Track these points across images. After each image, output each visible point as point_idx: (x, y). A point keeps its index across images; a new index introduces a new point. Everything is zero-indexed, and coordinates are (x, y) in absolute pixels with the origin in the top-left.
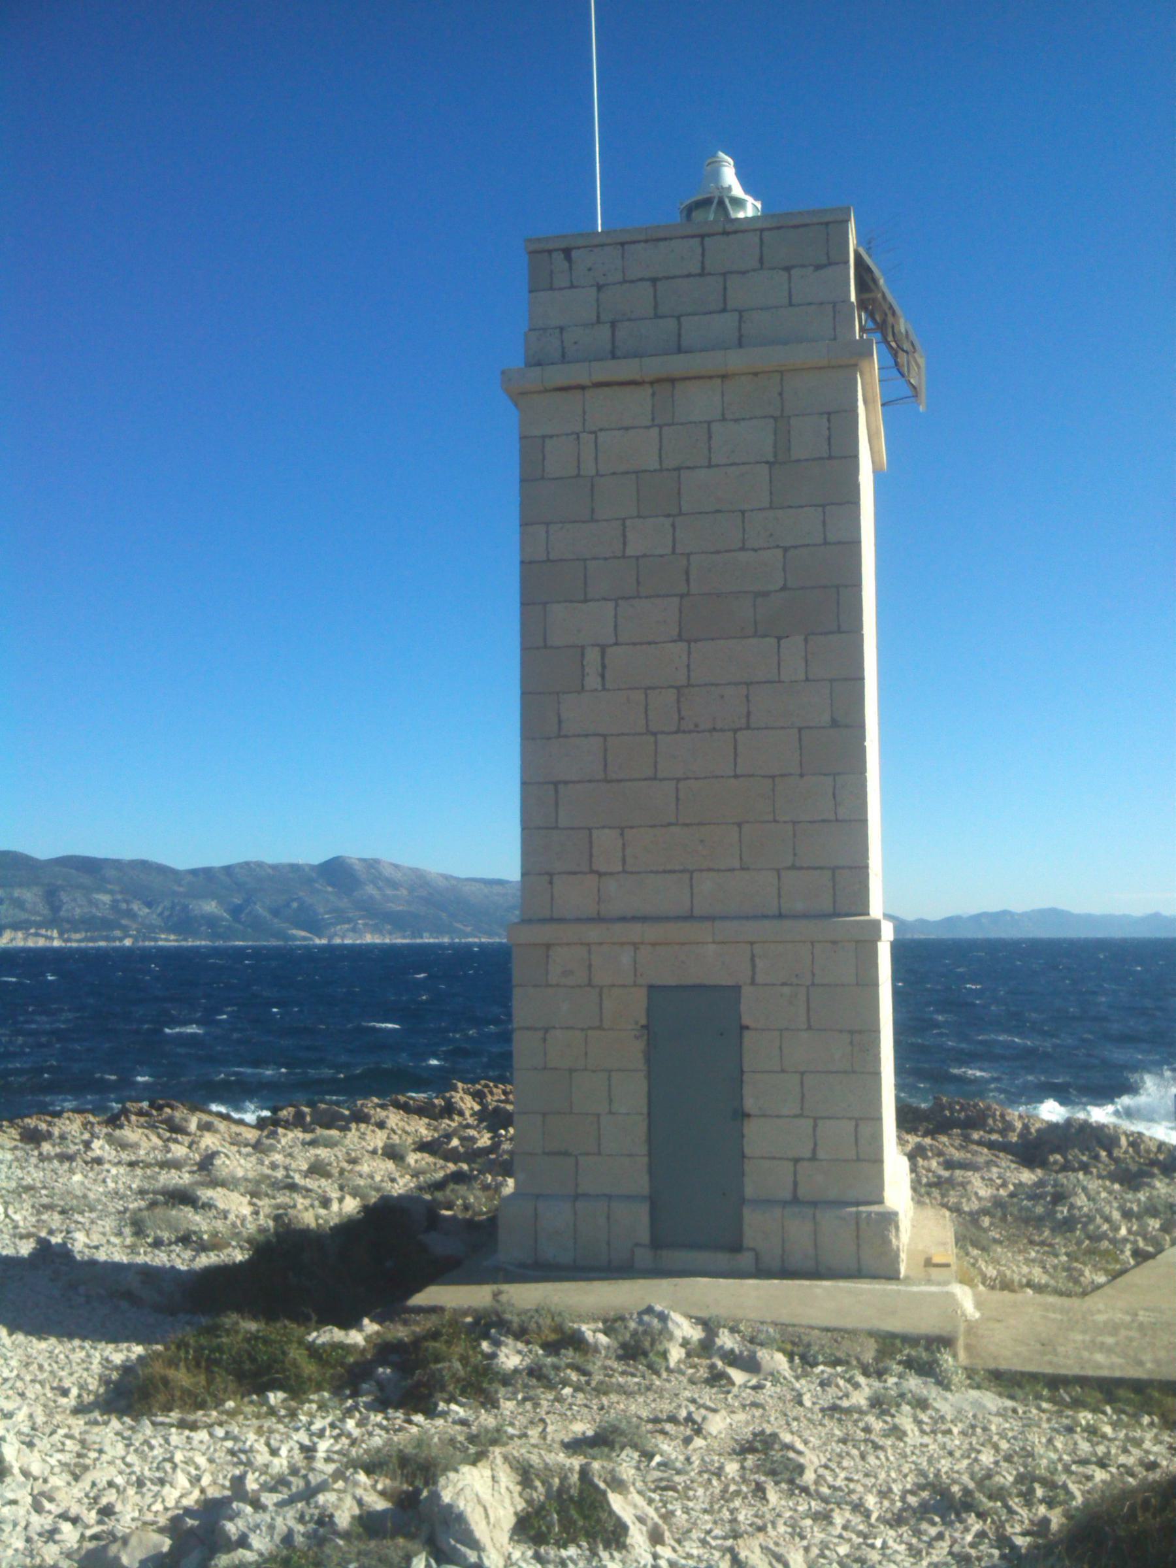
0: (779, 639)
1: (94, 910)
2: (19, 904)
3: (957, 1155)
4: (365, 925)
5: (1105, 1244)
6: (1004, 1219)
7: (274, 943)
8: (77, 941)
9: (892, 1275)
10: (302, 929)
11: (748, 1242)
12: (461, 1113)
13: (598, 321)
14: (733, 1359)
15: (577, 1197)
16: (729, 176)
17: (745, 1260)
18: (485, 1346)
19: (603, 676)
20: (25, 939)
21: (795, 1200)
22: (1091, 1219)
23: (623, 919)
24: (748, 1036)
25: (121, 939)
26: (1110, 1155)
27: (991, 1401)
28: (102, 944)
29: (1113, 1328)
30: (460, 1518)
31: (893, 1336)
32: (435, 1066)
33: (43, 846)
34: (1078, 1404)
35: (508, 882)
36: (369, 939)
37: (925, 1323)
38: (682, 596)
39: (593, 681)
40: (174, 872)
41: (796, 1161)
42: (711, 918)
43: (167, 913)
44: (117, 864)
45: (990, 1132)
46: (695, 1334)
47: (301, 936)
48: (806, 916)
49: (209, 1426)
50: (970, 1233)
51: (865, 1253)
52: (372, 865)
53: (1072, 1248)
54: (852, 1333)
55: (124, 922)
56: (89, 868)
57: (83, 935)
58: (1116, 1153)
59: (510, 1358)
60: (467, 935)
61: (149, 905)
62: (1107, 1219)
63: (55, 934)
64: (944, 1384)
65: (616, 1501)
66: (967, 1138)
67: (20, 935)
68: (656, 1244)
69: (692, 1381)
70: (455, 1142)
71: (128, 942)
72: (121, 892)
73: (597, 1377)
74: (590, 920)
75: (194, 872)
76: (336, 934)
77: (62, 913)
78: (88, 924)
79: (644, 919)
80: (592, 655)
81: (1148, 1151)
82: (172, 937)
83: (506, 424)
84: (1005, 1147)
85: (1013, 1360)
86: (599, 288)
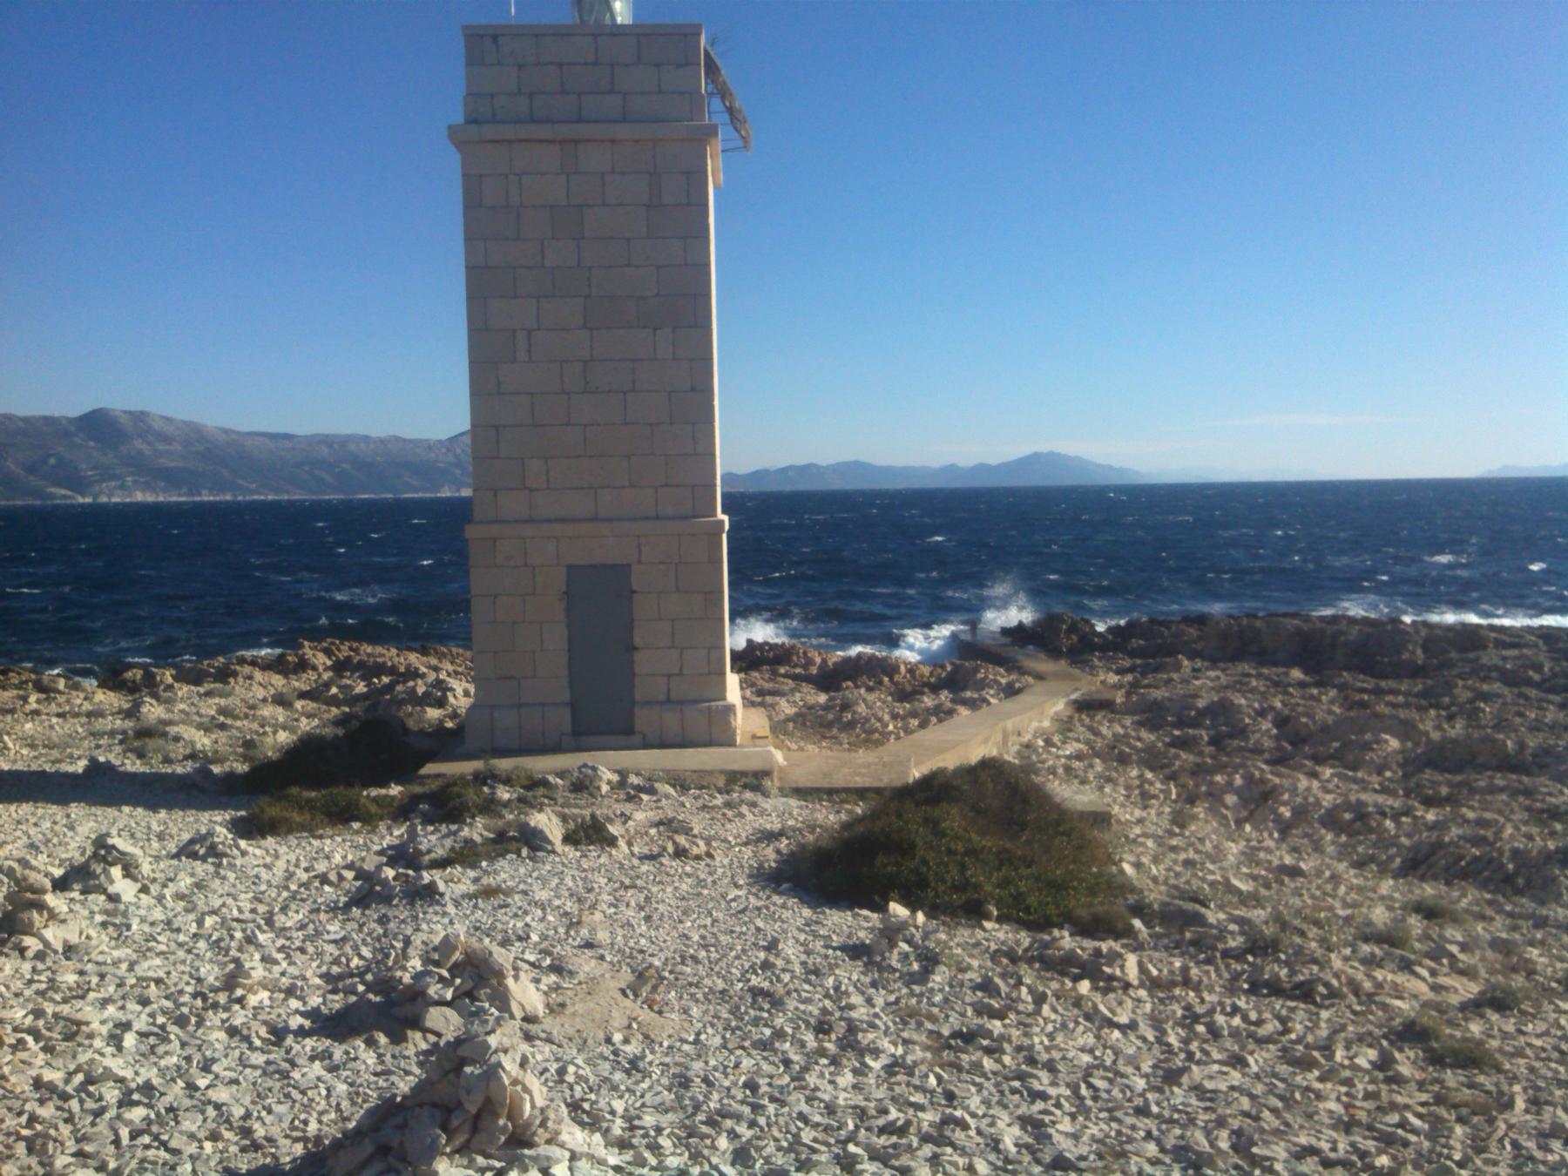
0: (655, 329)
3: (767, 686)
4: (134, 482)
6: (804, 724)
7: (30, 501)
9: (732, 743)
10: (59, 485)
11: (638, 727)
12: (315, 668)
14: (639, 789)
15: (520, 706)
17: (637, 739)
18: (486, 789)
21: (669, 701)
22: (867, 720)
23: (549, 521)
24: (636, 597)
26: (891, 680)
29: (868, 765)
30: (541, 832)
31: (735, 772)
34: (844, 801)
36: (139, 497)
41: (669, 676)
42: (610, 520)
45: (795, 666)
46: (615, 778)
47: (61, 495)
48: (674, 518)
51: (717, 732)
52: (140, 417)
53: (853, 739)
54: (711, 773)
58: (896, 678)
59: (504, 794)
60: (252, 492)
62: (880, 720)
64: (766, 794)
65: (611, 829)
66: (775, 673)
68: (576, 733)
69: (617, 801)
70: (334, 690)
74: (525, 522)
76: (101, 492)
79: (563, 520)
81: (922, 676)
83: (452, 162)
84: (808, 679)
85: (804, 782)
86: (520, 67)
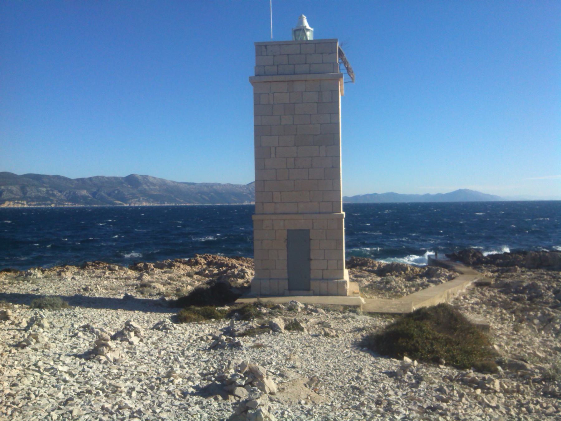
1: (39, 194)
2: (11, 192)
3: (359, 274)
4: (143, 199)
5: (399, 293)
6: (372, 288)
7: (109, 206)
8: (33, 205)
9: (346, 295)
11: (312, 288)
12: (201, 264)
13: (274, 65)
14: (312, 310)
15: (270, 279)
16: (306, 23)
17: (311, 292)
19: (275, 154)
20: (14, 205)
21: (323, 279)
22: (396, 287)
24: (312, 242)
25: (50, 205)
26: (405, 273)
27: (368, 317)
28: (43, 206)
29: (396, 305)
30: (277, 325)
32: (368, 247)
33: (19, 171)
34: (387, 318)
35: (196, 184)
36: (144, 204)
37: (354, 303)
38: (295, 135)
39: (273, 155)
40: (70, 180)
41: (323, 270)
42: (303, 213)
43: (67, 195)
44: (48, 177)
46: (303, 306)
47: (119, 203)
48: (325, 213)
49: (205, 324)
50: (363, 290)
51: (340, 290)
52: (145, 177)
53: (390, 295)
54: (338, 305)
55: (51, 198)
56: (37, 178)
57: (36, 203)
58: (407, 272)
59: (264, 311)
60: (181, 203)
61: (61, 192)
62: (400, 288)
63: (25, 202)
64: (358, 314)
66: (361, 269)
67: (12, 203)
68: (290, 289)
69: (304, 314)
70: (207, 272)
71: (53, 206)
72: (50, 187)
73: (284, 314)
74: (273, 214)
75: (77, 180)
76: (132, 203)
77: (27, 195)
78: (38, 199)
80: (273, 150)
82: (70, 204)
86: (274, 56)
